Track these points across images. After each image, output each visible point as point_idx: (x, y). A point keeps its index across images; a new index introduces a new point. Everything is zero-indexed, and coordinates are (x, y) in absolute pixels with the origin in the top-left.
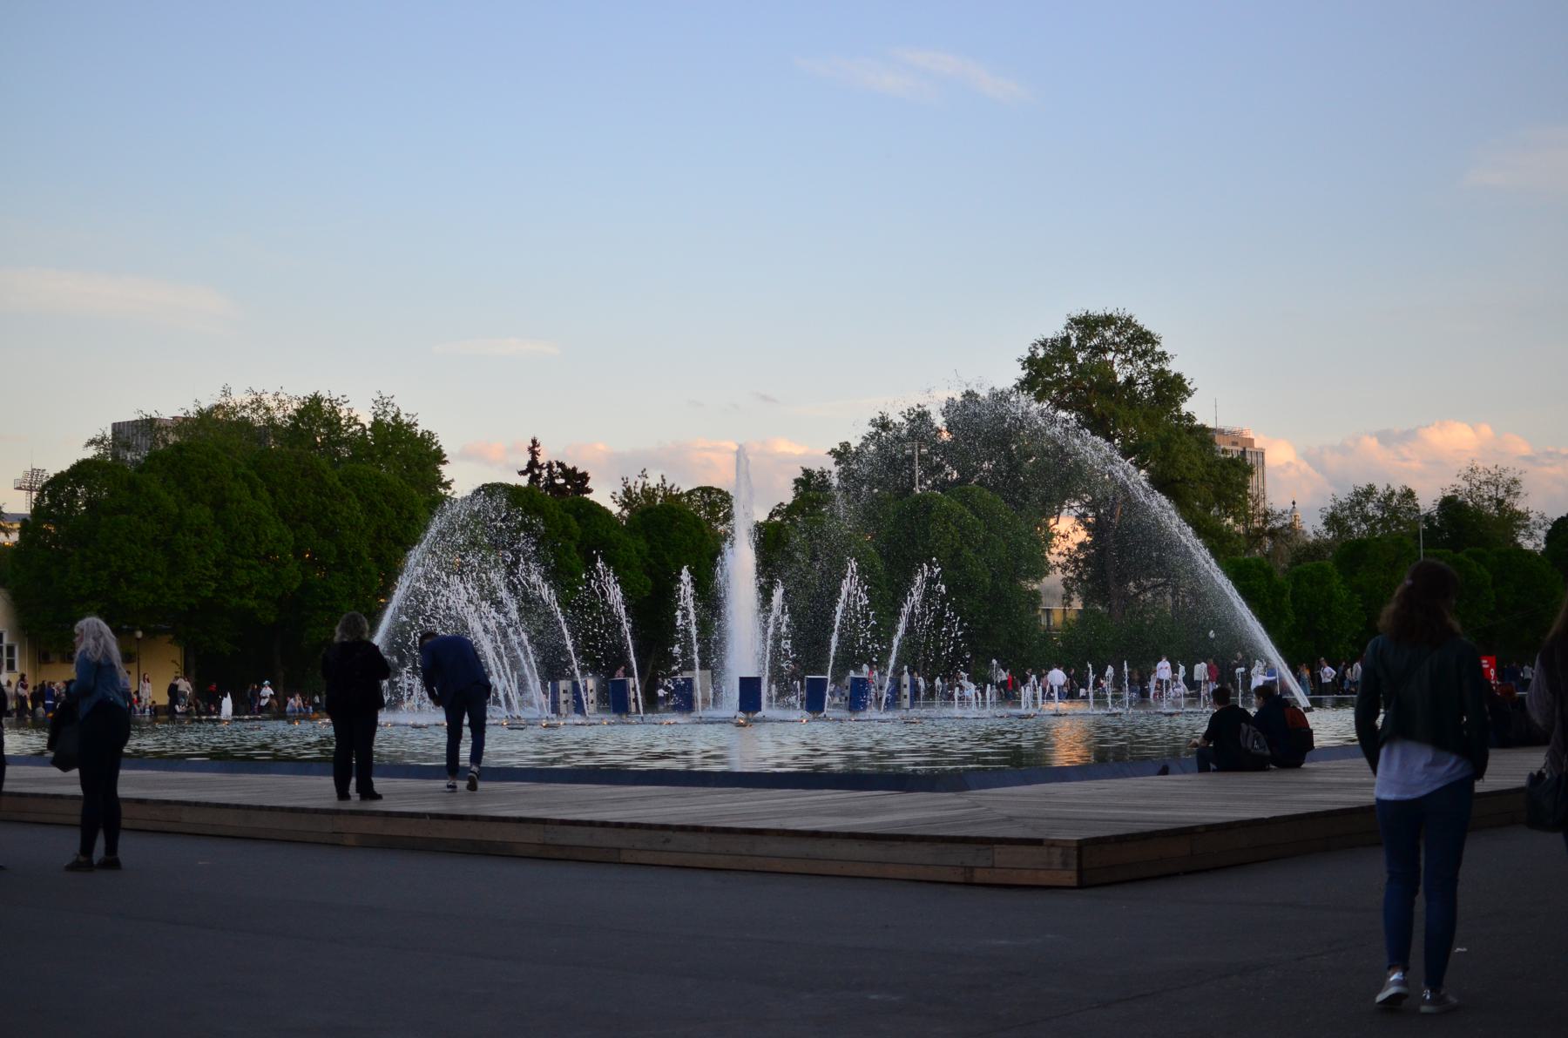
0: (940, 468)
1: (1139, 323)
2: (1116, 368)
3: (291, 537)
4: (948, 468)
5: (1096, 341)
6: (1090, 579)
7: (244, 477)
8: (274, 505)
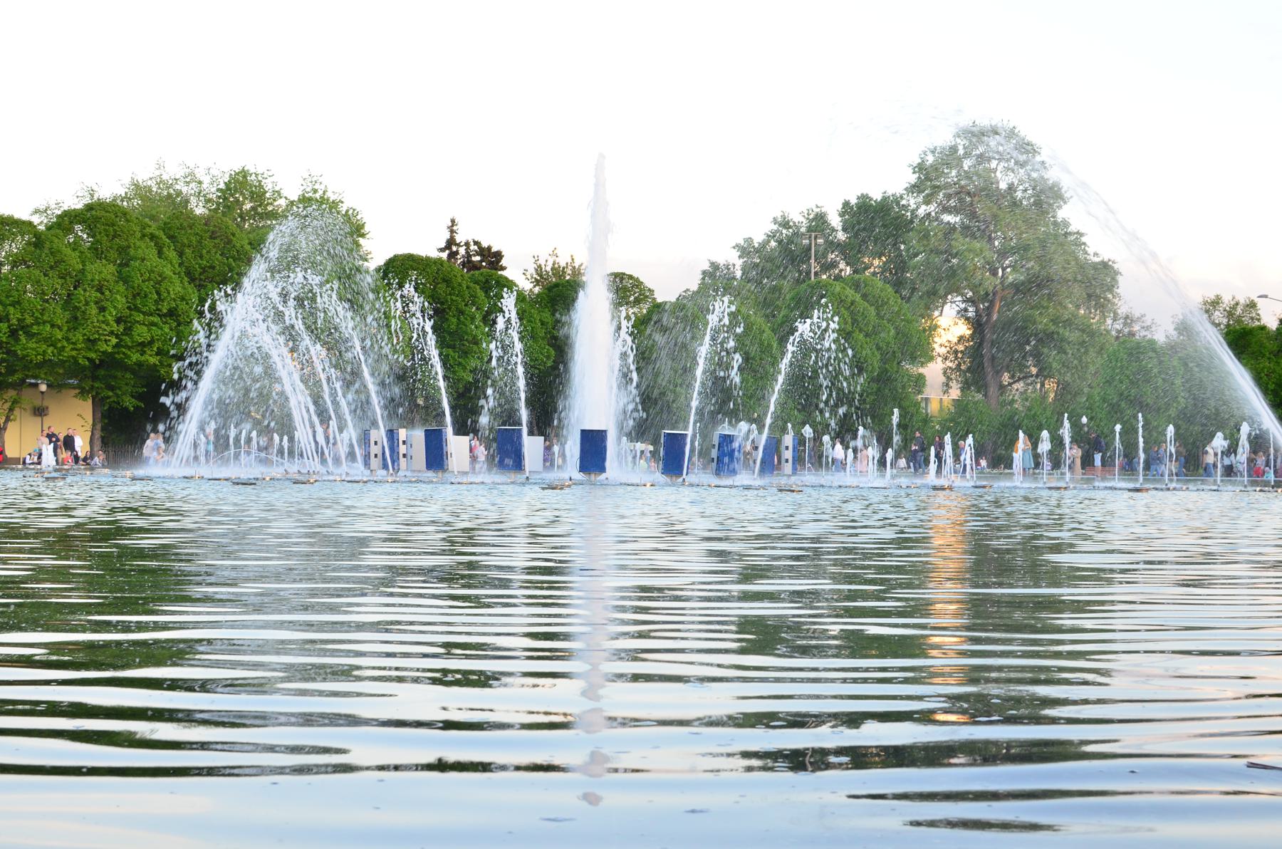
0: (834, 265)
1: (1022, 134)
2: (998, 174)
4: (842, 265)
5: (981, 149)
6: (969, 369)
7: (152, 237)
8: (180, 265)
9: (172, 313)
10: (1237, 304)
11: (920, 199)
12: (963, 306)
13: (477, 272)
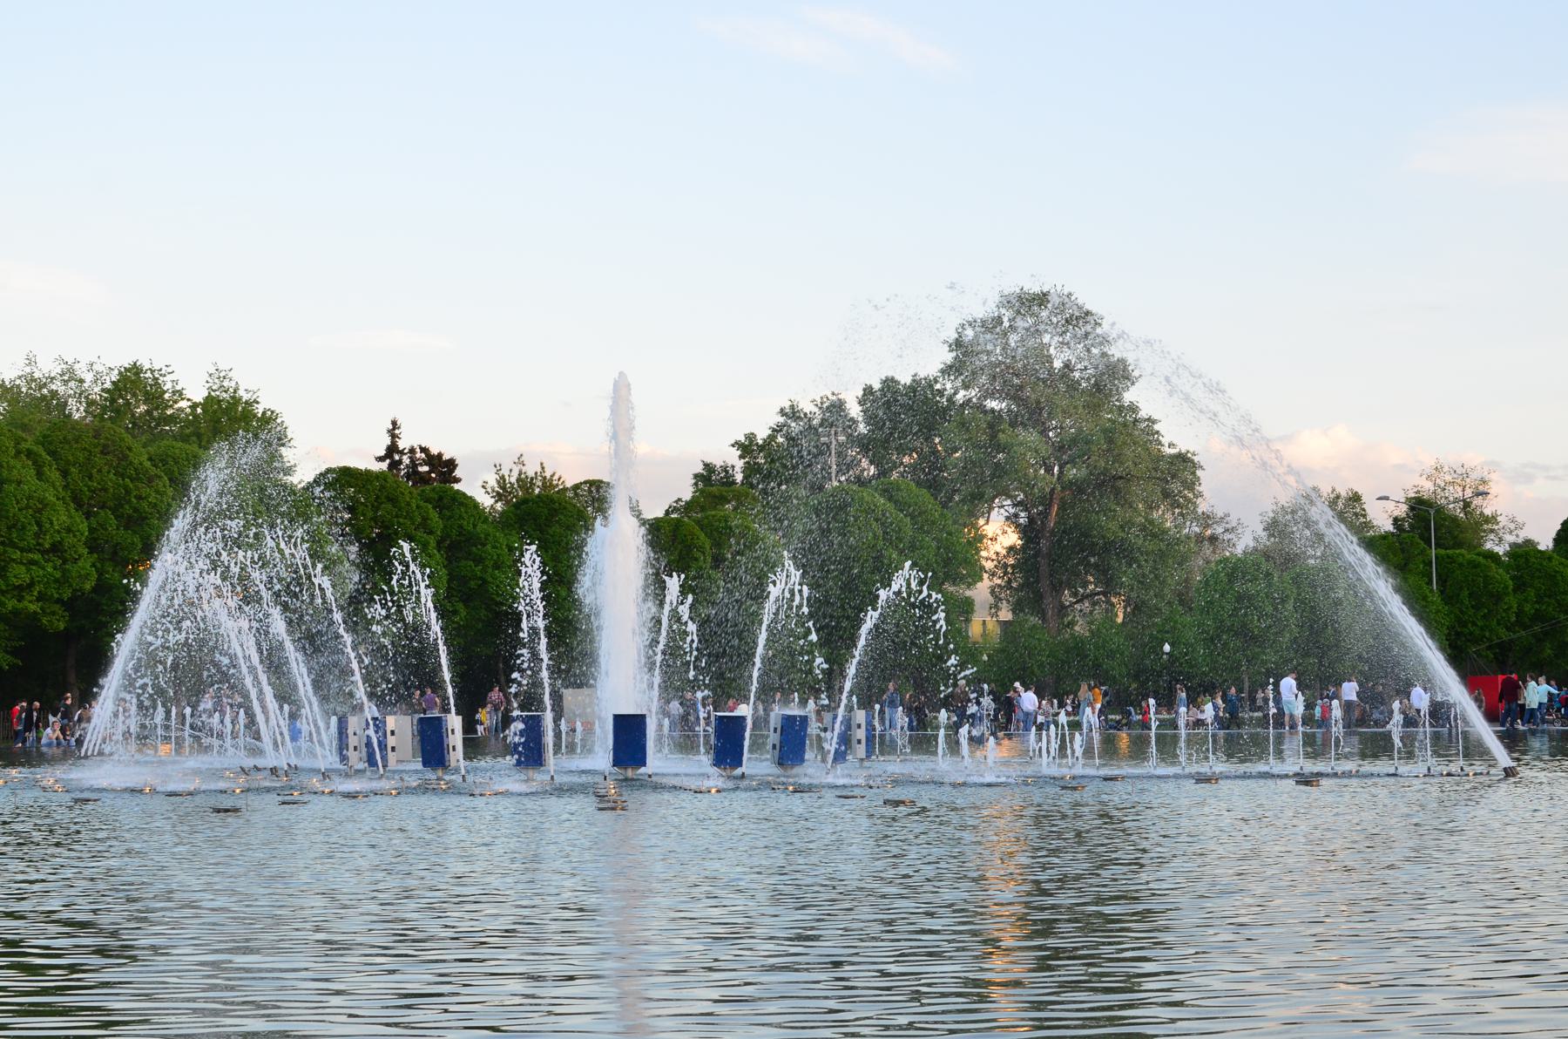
2: (1052, 351)
3: (84, 527)
4: (865, 463)
6: (1021, 587)
7: (29, 454)
8: (66, 487)
9: (56, 548)
10: (1338, 497)
11: (959, 383)
12: (1012, 511)
13: (428, 488)
